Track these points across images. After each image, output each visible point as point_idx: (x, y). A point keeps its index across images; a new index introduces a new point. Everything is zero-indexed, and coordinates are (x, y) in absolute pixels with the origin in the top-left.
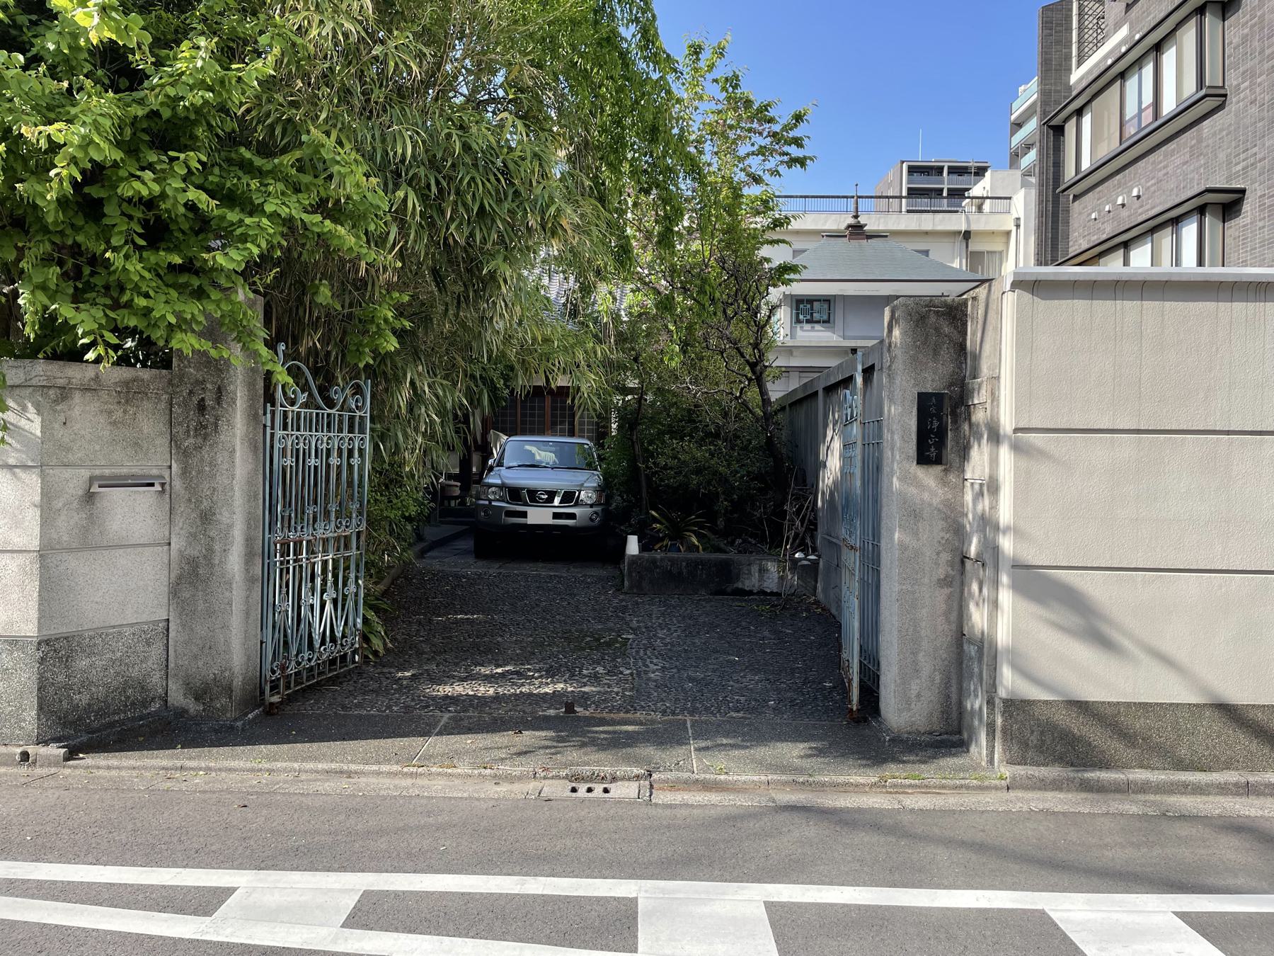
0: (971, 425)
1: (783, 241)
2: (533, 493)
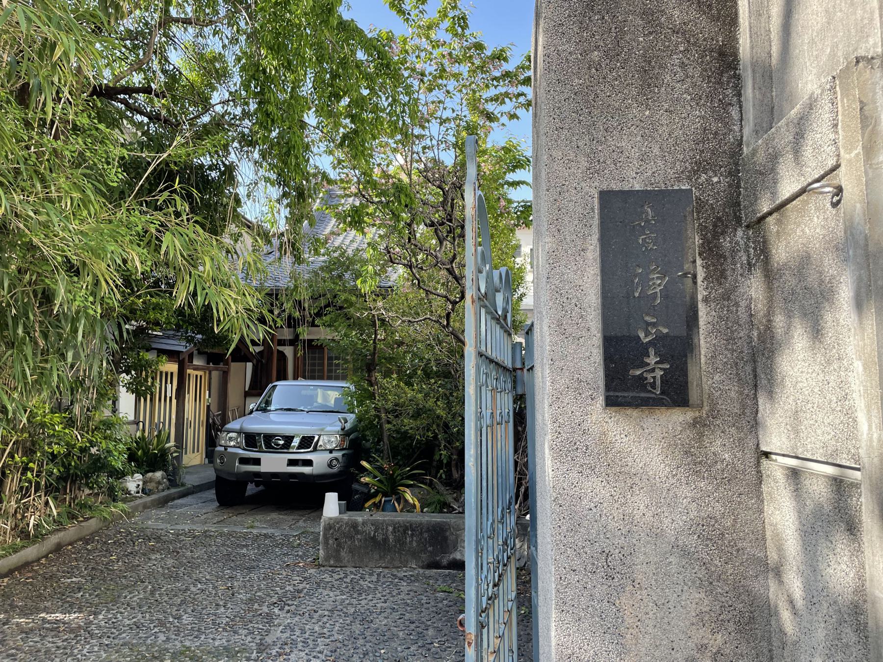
0: (770, 276)
1: (523, 183)
2: (269, 438)
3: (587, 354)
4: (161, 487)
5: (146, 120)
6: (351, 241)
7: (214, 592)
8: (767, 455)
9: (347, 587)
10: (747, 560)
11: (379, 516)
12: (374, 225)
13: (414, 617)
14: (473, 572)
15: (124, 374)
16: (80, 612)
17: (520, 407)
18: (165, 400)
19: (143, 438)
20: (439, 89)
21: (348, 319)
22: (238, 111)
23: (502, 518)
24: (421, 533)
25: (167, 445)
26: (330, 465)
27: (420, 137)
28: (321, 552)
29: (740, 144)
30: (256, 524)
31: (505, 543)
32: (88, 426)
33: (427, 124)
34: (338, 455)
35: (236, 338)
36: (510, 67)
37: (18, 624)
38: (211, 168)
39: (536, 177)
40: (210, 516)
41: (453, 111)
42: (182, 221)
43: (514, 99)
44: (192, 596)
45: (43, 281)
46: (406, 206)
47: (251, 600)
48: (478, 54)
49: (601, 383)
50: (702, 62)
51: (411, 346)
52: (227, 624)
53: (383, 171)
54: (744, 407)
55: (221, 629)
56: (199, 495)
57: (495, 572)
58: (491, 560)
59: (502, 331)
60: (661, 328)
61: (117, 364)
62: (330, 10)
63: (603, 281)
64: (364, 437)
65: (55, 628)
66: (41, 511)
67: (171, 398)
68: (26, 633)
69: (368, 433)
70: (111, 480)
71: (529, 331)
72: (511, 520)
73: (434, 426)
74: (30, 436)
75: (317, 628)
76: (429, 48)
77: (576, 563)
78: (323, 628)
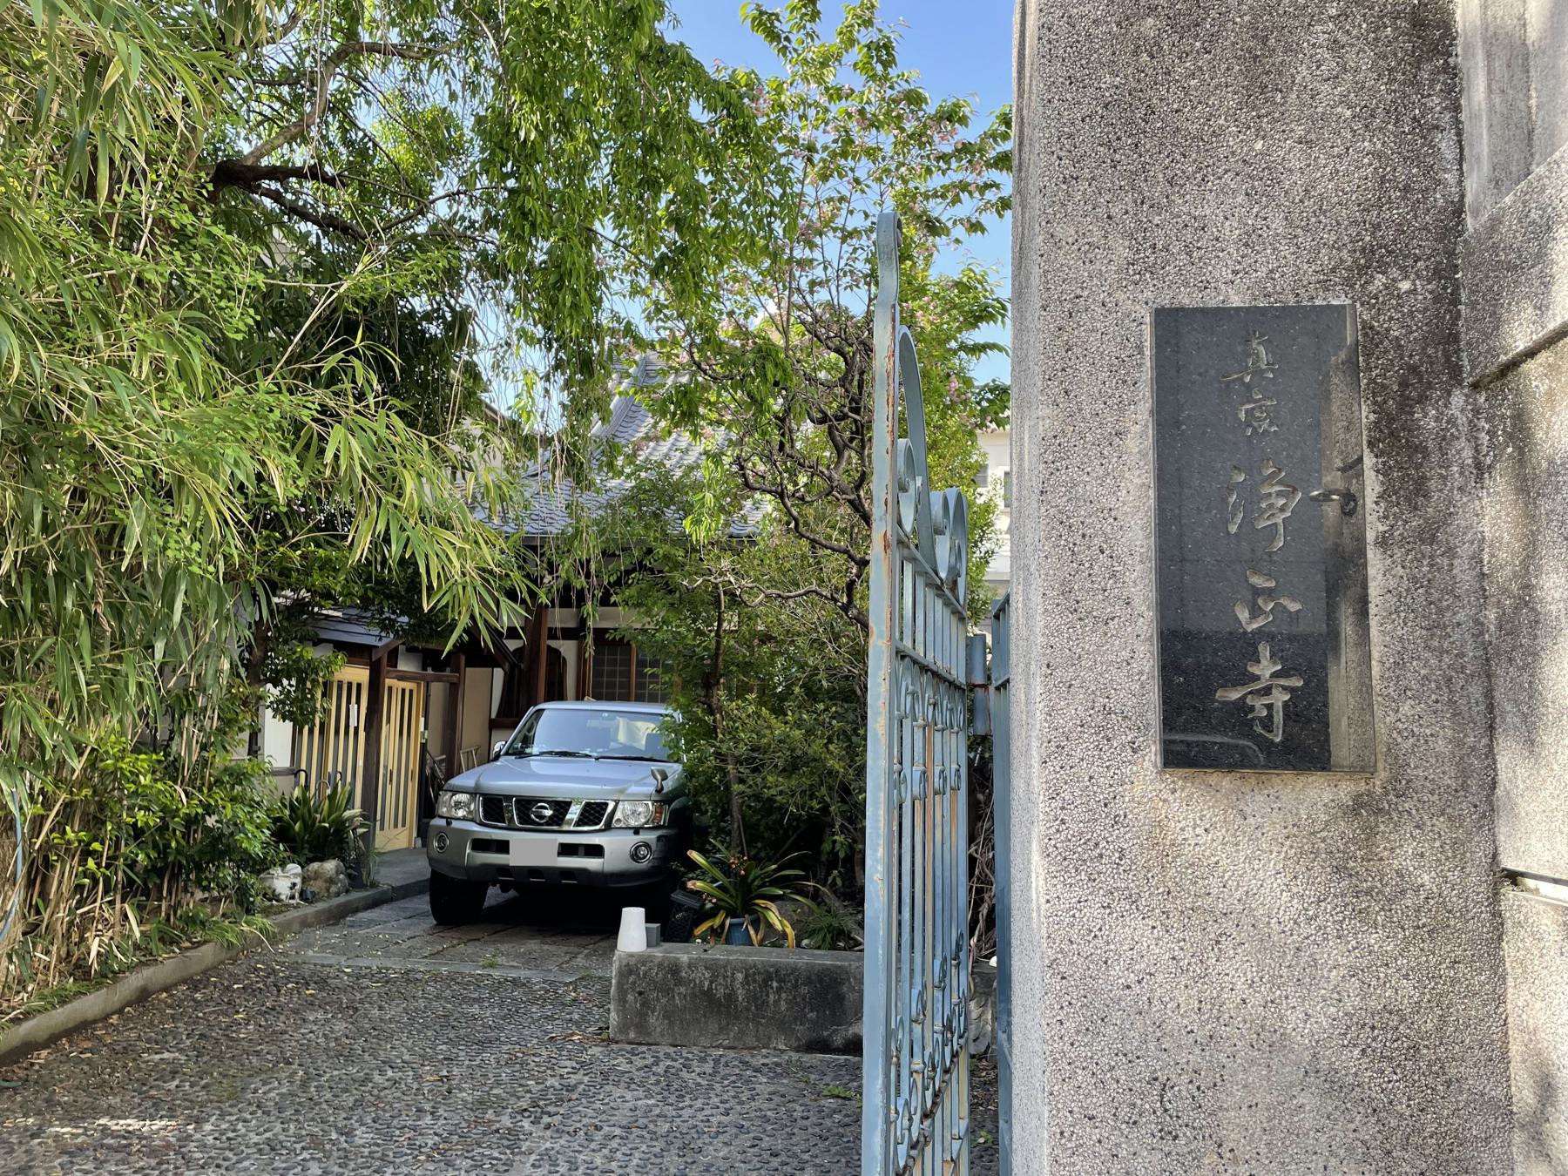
0: (1528, 486)
1: (993, 346)
2: (526, 805)
3: (1125, 654)
4: (333, 889)
5: (314, 229)
6: (681, 451)
7: (415, 1086)
8: (1514, 877)
9: (658, 1082)
10: (1467, 1104)
11: (719, 953)
12: (720, 423)
13: (779, 1145)
14: (879, 1100)
15: (269, 686)
16: (171, 1117)
17: (982, 758)
18: (347, 733)
19: (304, 800)
20: (841, 176)
21: (670, 592)
22: (477, 214)
23: (942, 980)
24: (796, 986)
25: (347, 814)
26: (635, 856)
27: (804, 264)
28: (613, 1015)
29: (1459, 211)
30: (501, 960)
31: (948, 1027)
32: (203, 778)
33: (817, 240)
34: (651, 837)
35: (464, 621)
36: (969, 134)
37: (57, 1137)
38: (427, 317)
39: (1020, 332)
40: (418, 942)
41: (867, 216)
42: (367, 406)
43: (977, 194)
44: (375, 1092)
45: (112, 512)
46: (776, 384)
47: (481, 1104)
48: (912, 111)
49: (1154, 717)
50: (1377, 39)
51: (784, 642)
52: (435, 1147)
53: (738, 326)
54: (1464, 773)
55: (422, 1158)
56: (402, 903)
57: (925, 1088)
58: (919, 1067)
59: (947, 612)
60: (1284, 601)
61: (255, 668)
62: (633, 17)
63: (1161, 499)
64: (697, 806)
65: (123, 1146)
66: (114, 929)
67: (356, 729)
68: (71, 1154)
69: (703, 799)
70: (243, 875)
71: (1001, 612)
72: (961, 980)
73: (823, 790)
74: (95, 792)
75: (598, 1161)
76: (823, 100)
77: (1097, 1102)
78: (611, 1160)
